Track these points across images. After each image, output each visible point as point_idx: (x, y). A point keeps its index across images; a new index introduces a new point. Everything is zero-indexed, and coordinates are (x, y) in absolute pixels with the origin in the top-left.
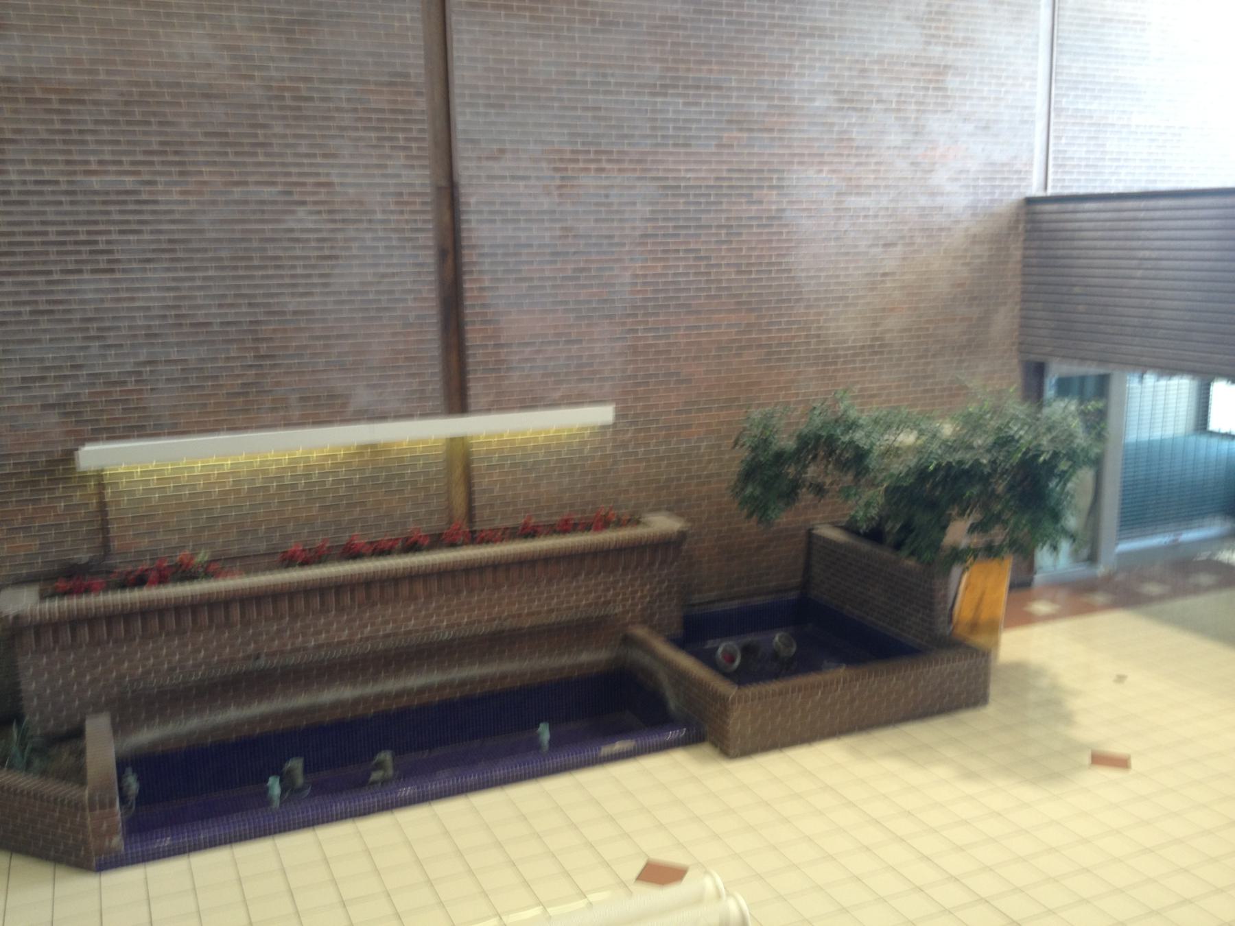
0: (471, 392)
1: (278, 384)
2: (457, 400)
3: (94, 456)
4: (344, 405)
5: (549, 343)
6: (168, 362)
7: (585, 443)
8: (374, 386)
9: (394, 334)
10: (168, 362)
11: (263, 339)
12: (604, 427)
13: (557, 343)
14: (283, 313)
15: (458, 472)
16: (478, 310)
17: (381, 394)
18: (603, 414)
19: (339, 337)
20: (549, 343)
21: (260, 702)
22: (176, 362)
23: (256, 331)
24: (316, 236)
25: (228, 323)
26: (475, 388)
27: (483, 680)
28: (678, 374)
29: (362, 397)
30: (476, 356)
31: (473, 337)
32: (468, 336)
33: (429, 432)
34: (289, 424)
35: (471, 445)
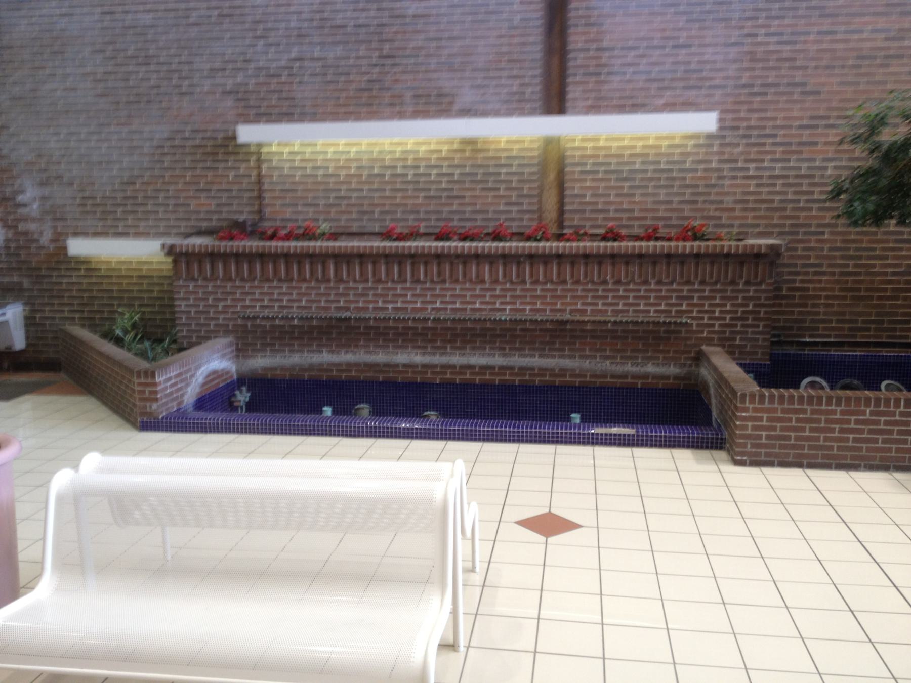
0: (570, 96)
1: (396, 81)
2: (555, 101)
3: (247, 133)
4: (451, 103)
5: (656, 47)
6: (313, 59)
7: (689, 154)
8: (479, 86)
9: (500, 37)
10: (313, 59)
11: (386, 41)
12: (709, 136)
13: (663, 47)
14: (405, 17)
15: (552, 176)
16: (581, 12)
17: (484, 94)
18: (705, 122)
19: (450, 39)
20: (656, 47)
21: (347, 352)
22: (319, 59)
23: (381, 33)
24: (894, 238)
25: (360, 26)
26: (573, 92)
27: (543, 371)
28: (804, 84)
29: (467, 97)
30: (577, 60)
31: (576, 40)
32: (571, 39)
33: (519, 132)
34: (401, 115)
35: (565, 150)
